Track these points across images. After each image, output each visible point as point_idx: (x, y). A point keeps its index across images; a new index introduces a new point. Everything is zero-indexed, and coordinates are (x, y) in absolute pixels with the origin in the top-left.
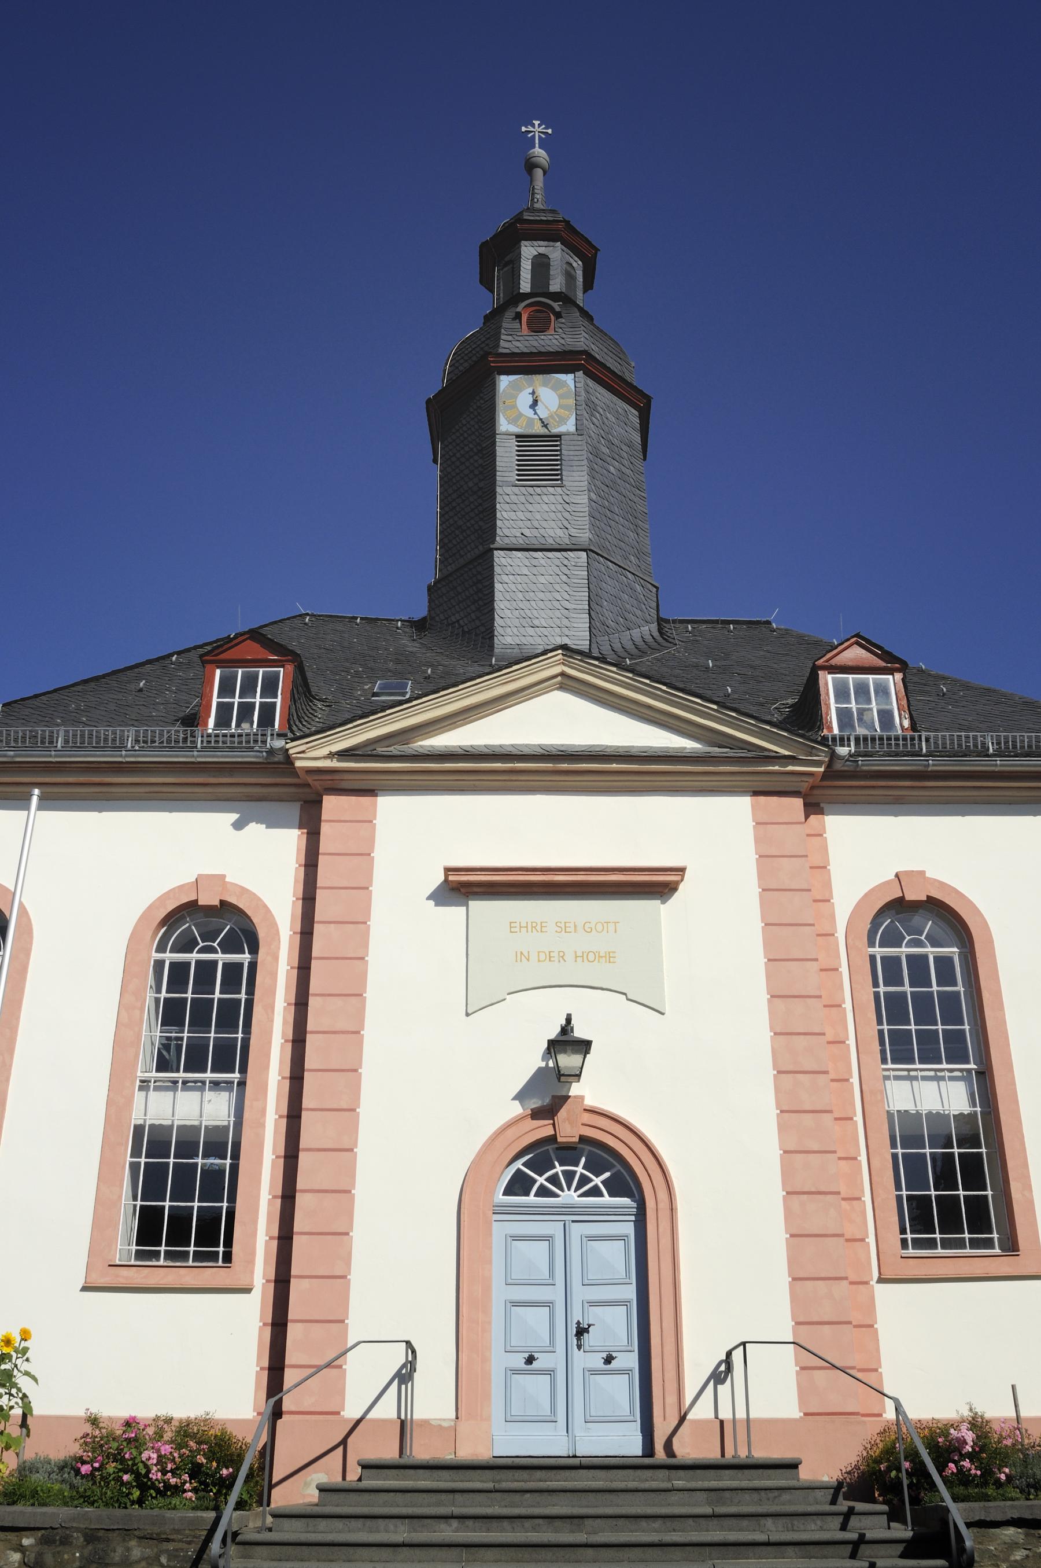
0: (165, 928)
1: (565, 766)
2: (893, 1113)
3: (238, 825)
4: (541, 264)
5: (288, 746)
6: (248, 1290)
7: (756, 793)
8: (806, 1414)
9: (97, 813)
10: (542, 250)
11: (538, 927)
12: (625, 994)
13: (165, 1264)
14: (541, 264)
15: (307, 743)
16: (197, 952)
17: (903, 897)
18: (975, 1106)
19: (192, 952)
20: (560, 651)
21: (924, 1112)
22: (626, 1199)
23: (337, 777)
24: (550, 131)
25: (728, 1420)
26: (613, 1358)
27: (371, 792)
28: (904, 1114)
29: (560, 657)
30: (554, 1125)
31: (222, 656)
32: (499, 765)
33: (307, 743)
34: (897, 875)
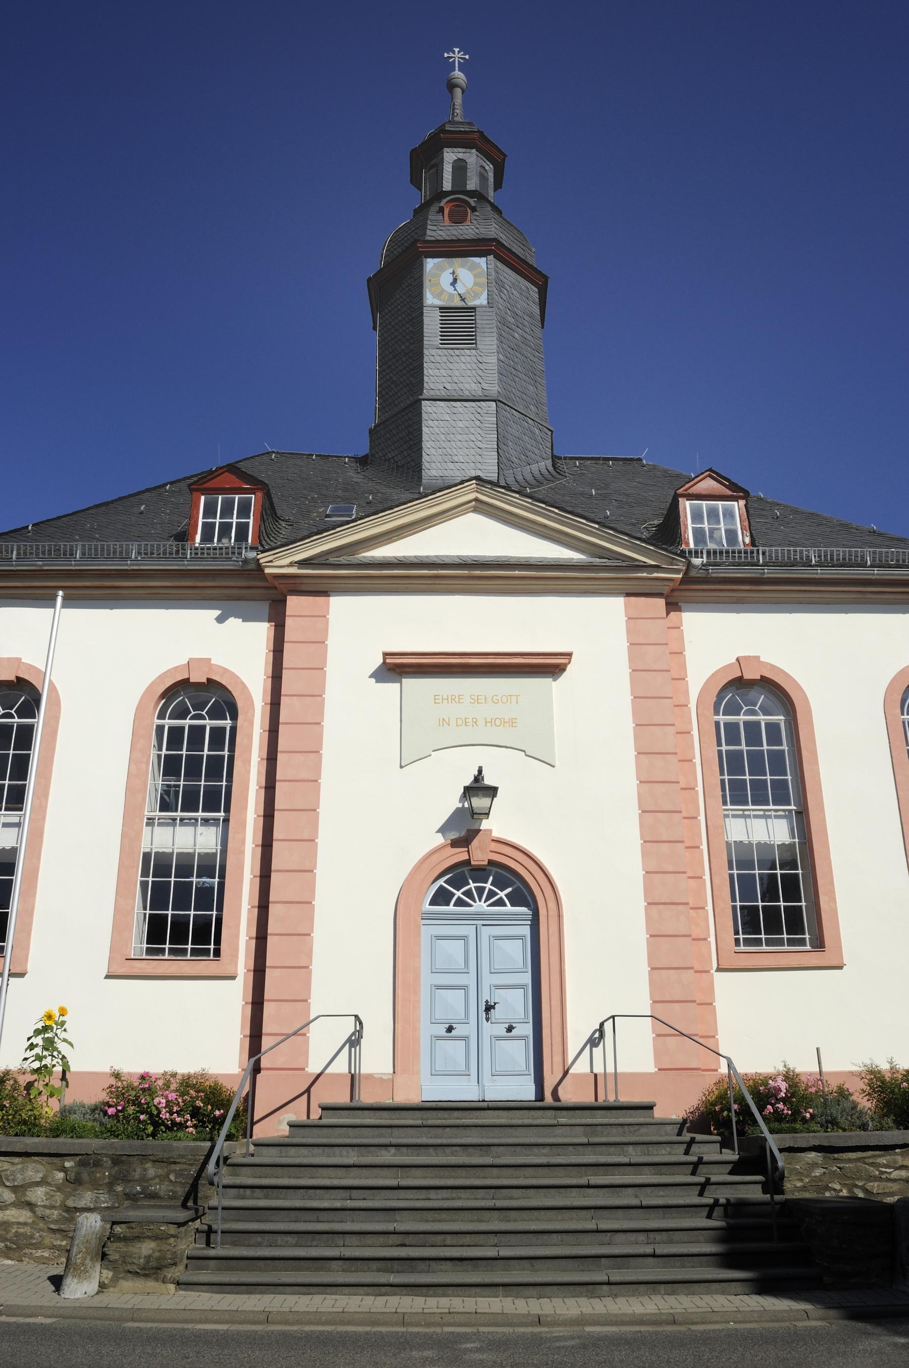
0: (164, 700)
1: (477, 573)
2: (731, 843)
3: (220, 620)
4: (460, 168)
5: (259, 557)
6: (233, 978)
7: (628, 595)
8: (659, 1070)
9: (109, 610)
10: (461, 156)
11: (456, 699)
12: (524, 751)
13: (169, 958)
14: (460, 168)
15: (274, 554)
16: (190, 719)
17: (189, 679)
18: (794, 837)
19: (186, 719)
20: (474, 482)
21: (755, 843)
22: (524, 908)
23: (298, 581)
24: (467, 57)
25: (600, 1074)
26: (513, 1028)
27: (325, 593)
28: (739, 844)
29: (474, 486)
30: (468, 851)
31: (204, 486)
32: (426, 572)
33: (274, 554)
34: (738, 660)
